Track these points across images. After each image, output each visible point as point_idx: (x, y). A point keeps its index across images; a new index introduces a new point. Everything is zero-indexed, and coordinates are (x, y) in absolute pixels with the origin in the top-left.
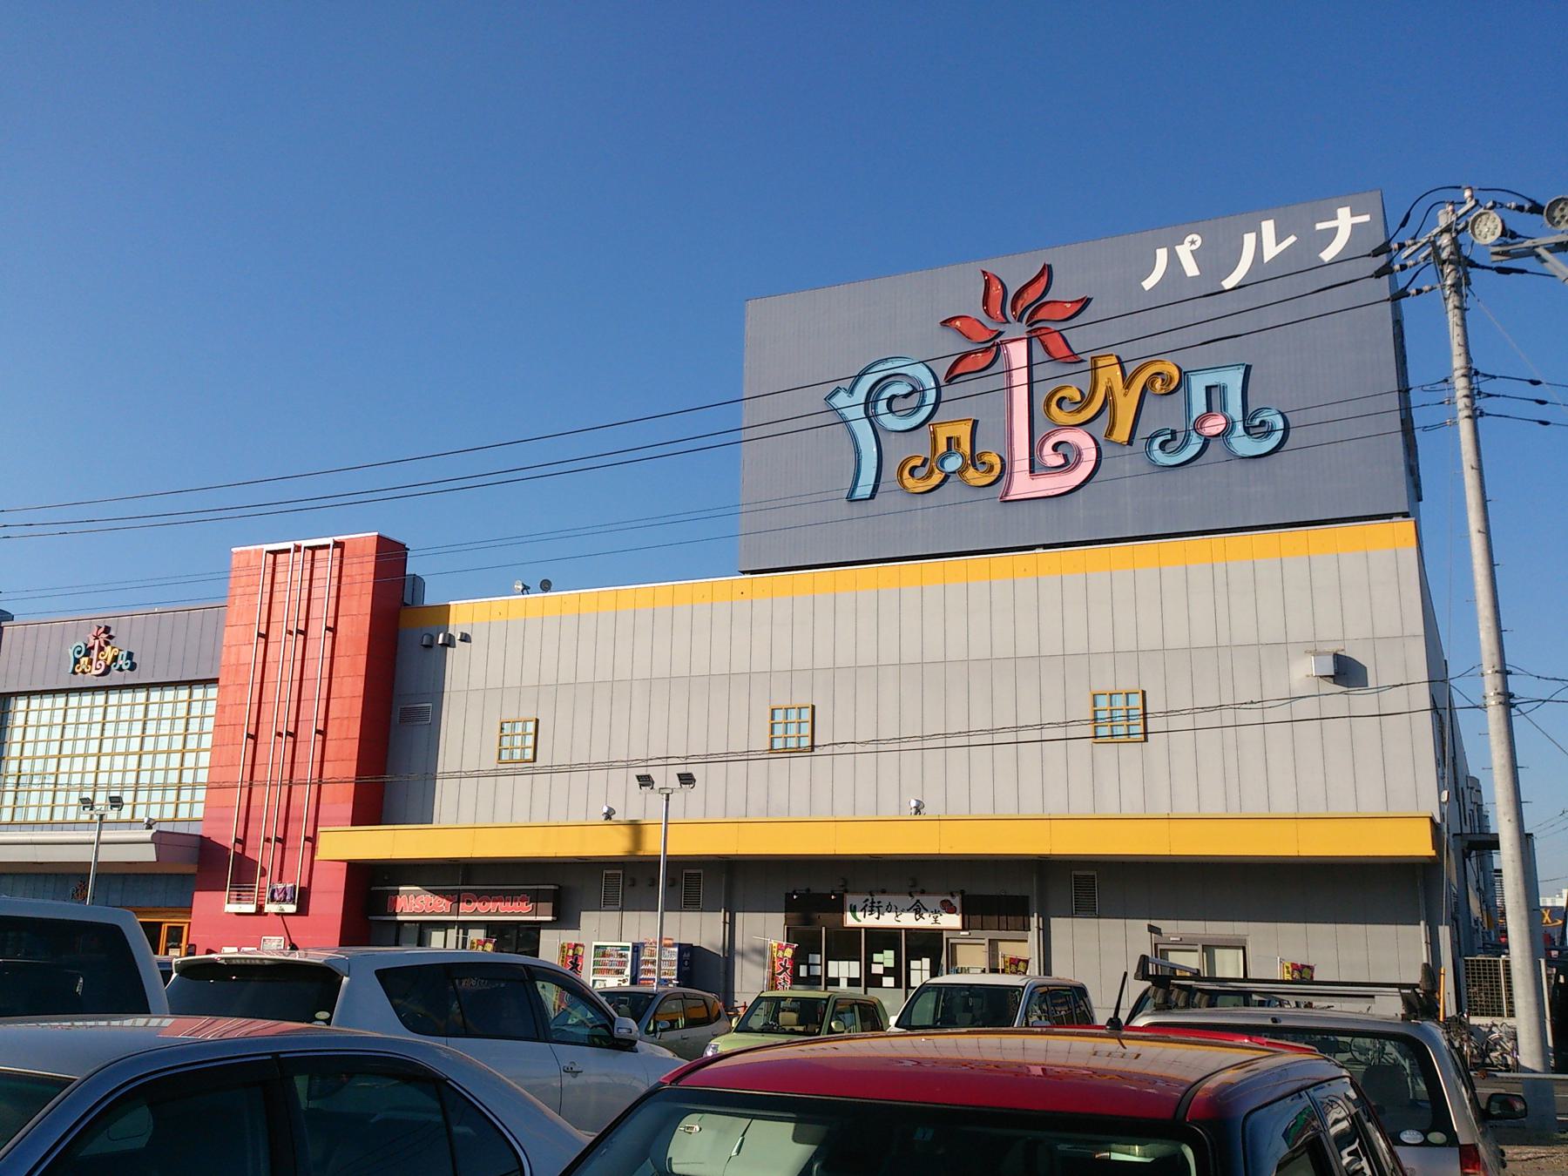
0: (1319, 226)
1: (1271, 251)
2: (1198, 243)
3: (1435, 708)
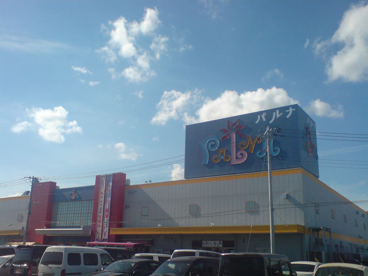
0: (286, 111)
1: (278, 116)
2: (265, 114)
3: (272, 198)
